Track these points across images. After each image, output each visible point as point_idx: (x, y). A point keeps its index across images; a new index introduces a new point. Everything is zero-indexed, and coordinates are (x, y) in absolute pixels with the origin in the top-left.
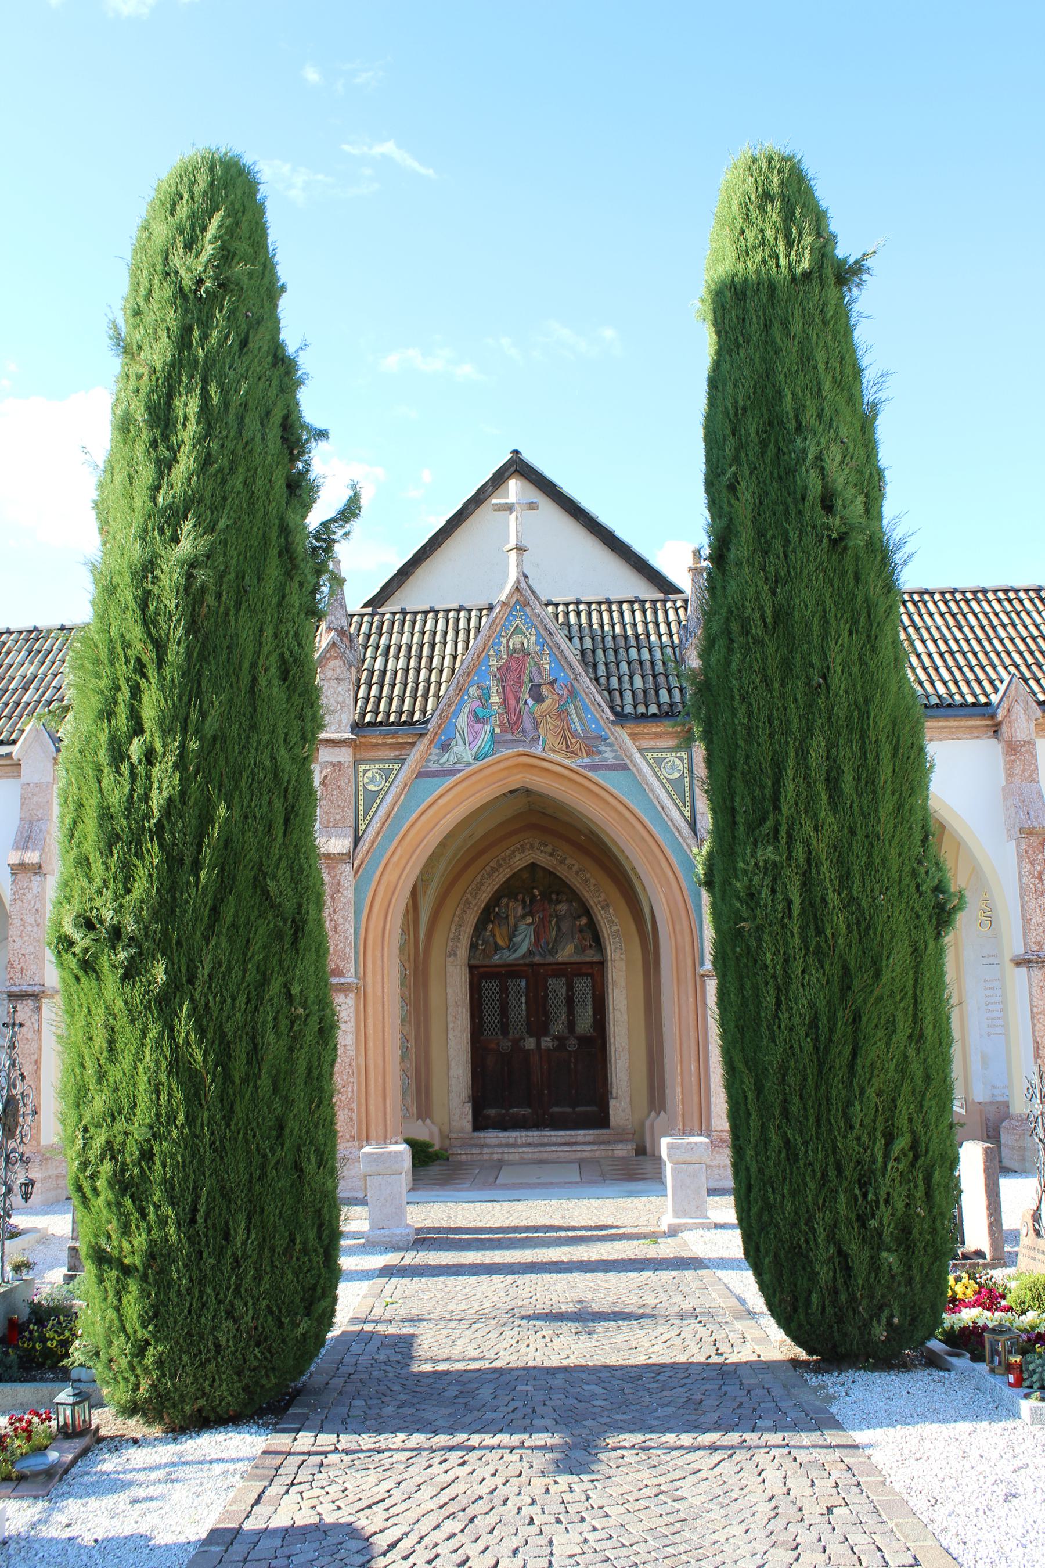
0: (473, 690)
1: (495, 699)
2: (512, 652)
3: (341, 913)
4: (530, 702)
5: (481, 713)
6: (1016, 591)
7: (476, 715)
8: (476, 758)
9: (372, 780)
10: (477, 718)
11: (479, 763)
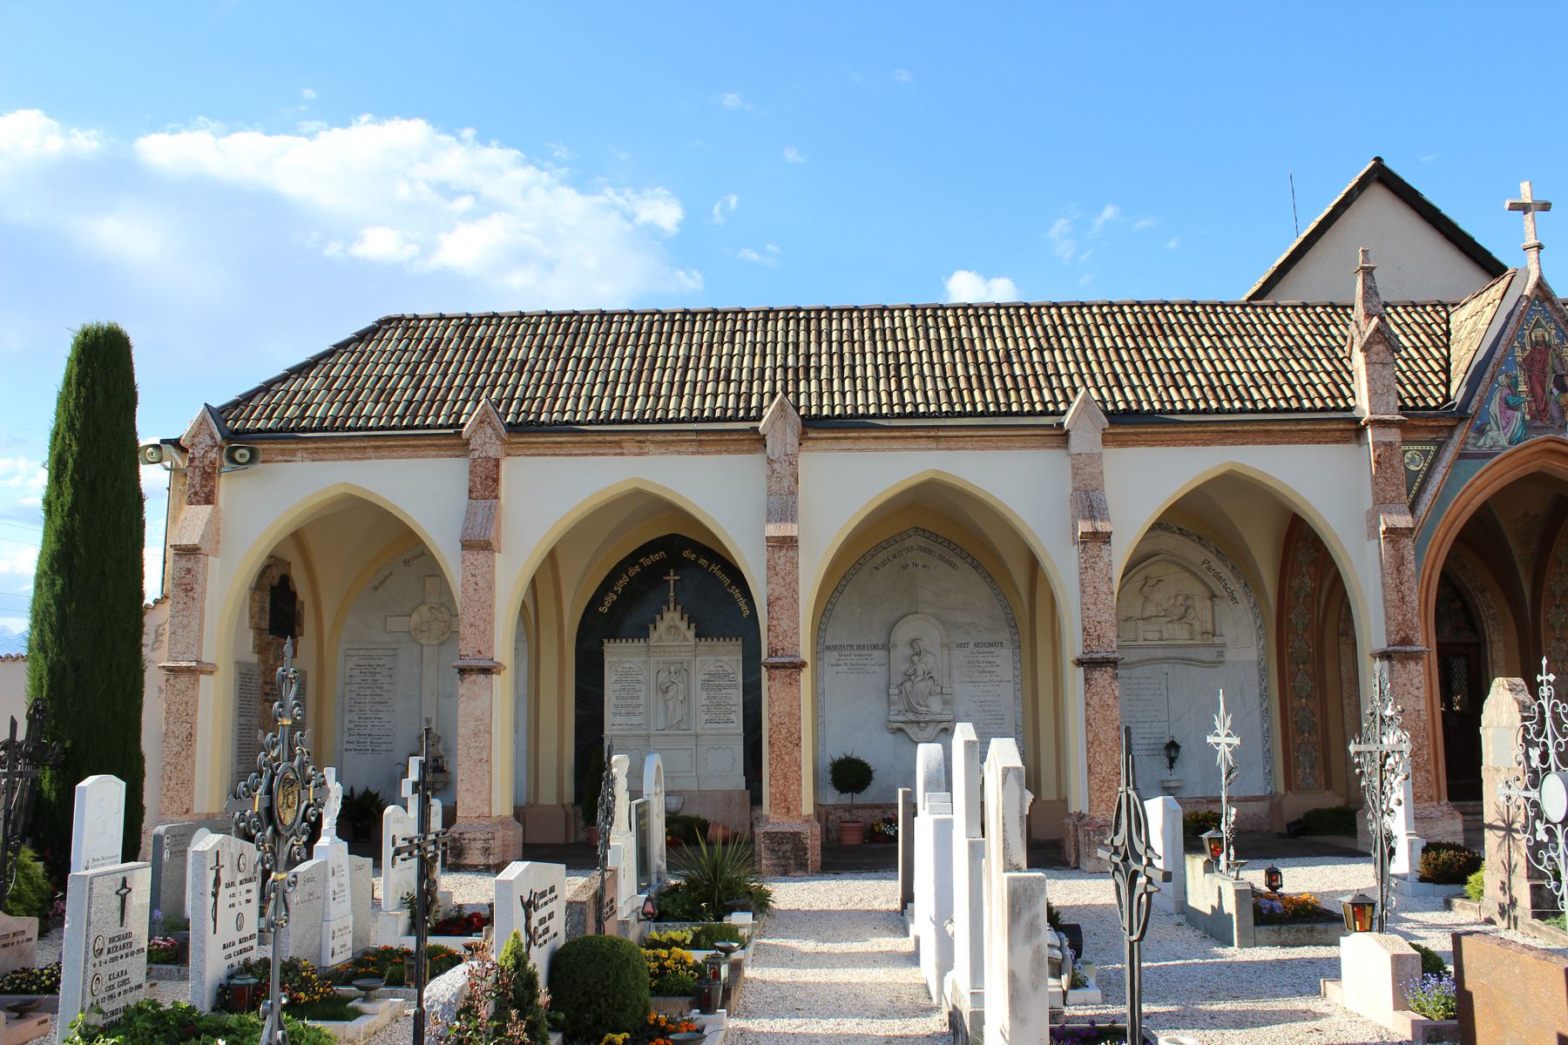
0: (1502, 378)
1: (1522, 388)
2: (1534, 345)
3: (1407, 585)
4: (1555, 391)
5: (1511, 401)
6: (1172, 306)
7: (1507, 402)
8: (1510, 443)
9: (1412, 460)
10: (1509, 406)
11: (1514, 448)
